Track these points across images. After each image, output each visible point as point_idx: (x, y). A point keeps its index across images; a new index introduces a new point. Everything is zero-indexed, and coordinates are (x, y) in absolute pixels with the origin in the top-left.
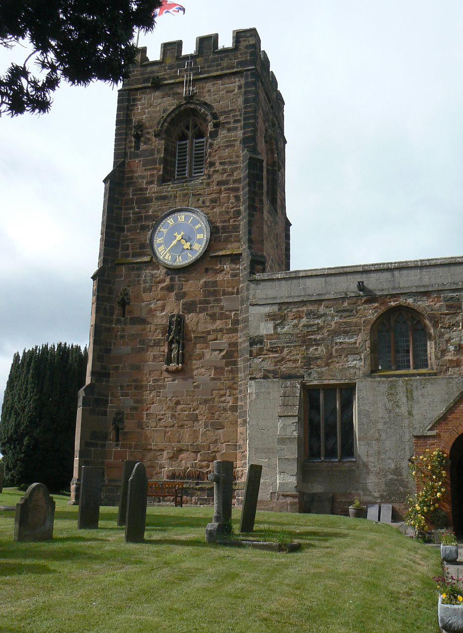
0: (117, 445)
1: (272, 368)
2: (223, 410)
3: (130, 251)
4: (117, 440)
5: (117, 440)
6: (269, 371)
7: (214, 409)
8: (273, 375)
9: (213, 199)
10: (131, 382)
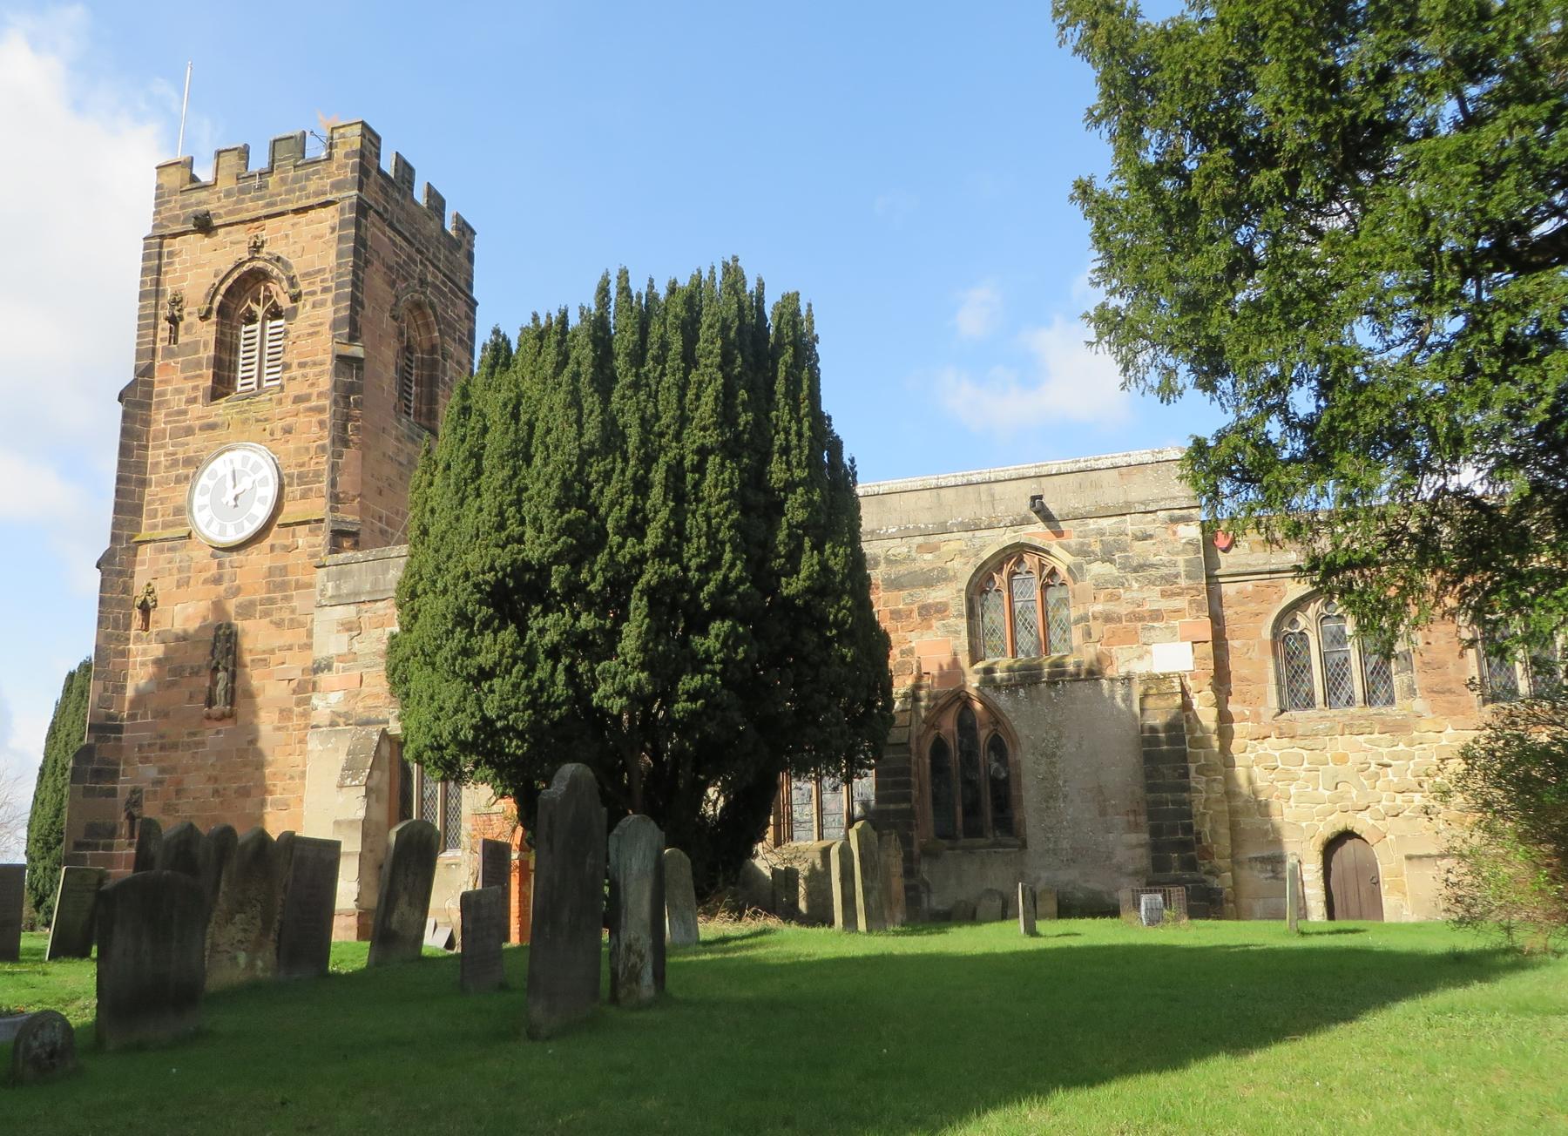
3: (159, 520)
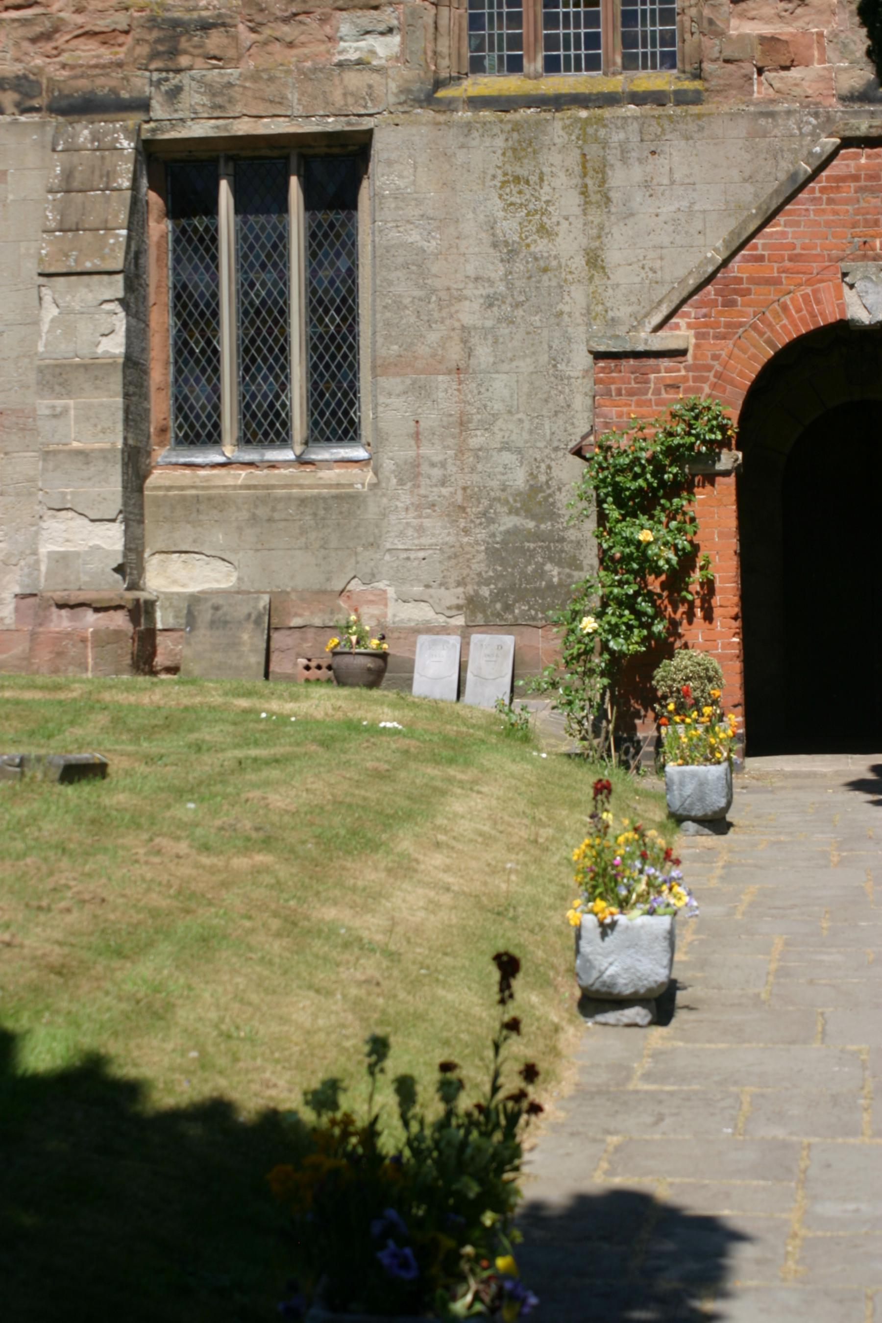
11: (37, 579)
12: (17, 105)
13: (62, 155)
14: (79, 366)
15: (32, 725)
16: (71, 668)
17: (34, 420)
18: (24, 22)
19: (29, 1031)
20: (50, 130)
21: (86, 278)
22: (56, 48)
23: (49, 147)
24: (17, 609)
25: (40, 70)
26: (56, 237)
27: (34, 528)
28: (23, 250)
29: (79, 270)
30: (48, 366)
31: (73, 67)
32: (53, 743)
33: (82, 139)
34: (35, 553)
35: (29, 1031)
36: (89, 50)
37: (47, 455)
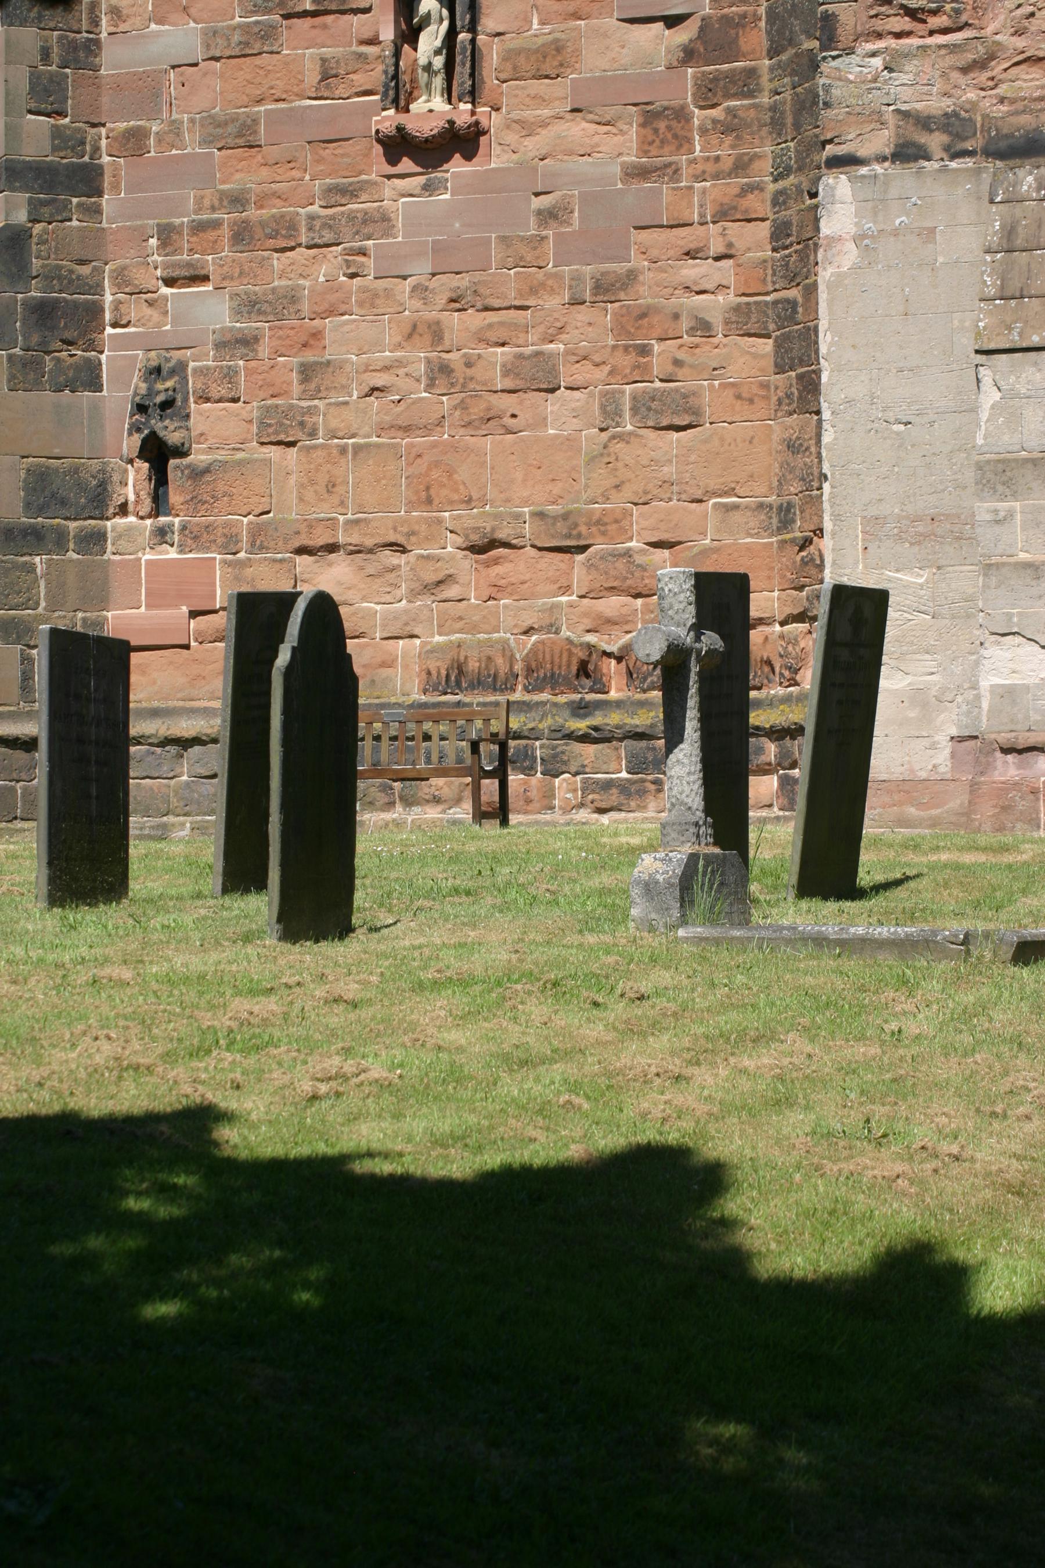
0: (162, 534)
1: (936, 105)
2: (691, 332)
4: (159, 504)
5: (159, 504)
6: (925, 122)
7: (651, 326)
8: (945, 138)
9: (301, 378)
10: (213, 209)
11: (978, 718)
12: (947, 149)
13: (1001, 206)
14: (1026, 461)
15: (977, 894)
16: (1019, 825)
17: (973, 528)
18: (953, 49)
19: (984, 1263)
20: (986, 177)
21: (1032, 355)
22: (992, 79)
23: (987, 199)
24: (953, 755)
25: (974, 105)
26: (996, 306)
27: (974, 657)
28: (956, 323)
29: (1024, 345)
30: (988, 462)
31: (1013, 101)
32: (1003, 915)
33: (1025, 188)
34: (975, 687)
35: (984, 1263)
36: (1032, 80)
37: (988, 568)
